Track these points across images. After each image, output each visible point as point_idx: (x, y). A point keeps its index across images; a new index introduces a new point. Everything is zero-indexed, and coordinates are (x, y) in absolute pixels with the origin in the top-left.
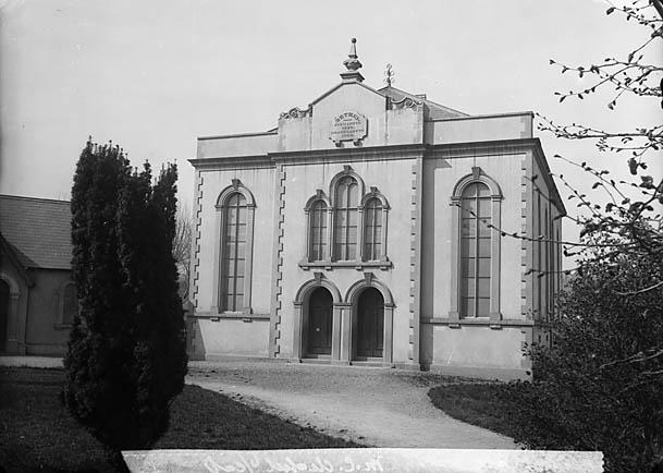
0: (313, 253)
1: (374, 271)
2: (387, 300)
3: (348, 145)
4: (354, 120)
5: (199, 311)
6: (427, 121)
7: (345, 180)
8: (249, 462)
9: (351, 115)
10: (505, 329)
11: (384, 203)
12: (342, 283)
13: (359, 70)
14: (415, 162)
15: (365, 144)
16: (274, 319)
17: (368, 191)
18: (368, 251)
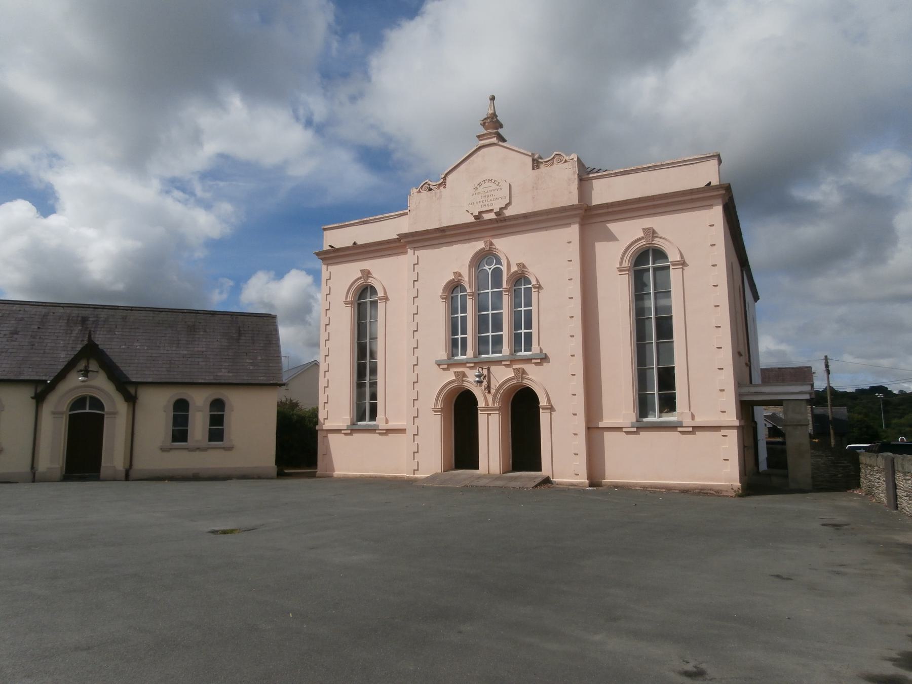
0: (456, 345)
1: (527, 367)
2: (543, 402)
3: (487, 217)
4: (494, 186)
5: (328, 425)
6: (585, 176)
7: (486, 255)
8: (45, 364)
9: (490, 181)
10: (699, 434)
11: (534, 282)
12: (261, 332)
13: (500, 131)
14: (573, 231)
15: (508, 213)
16: (411, 430)
17: (514, 268)
18: (522, 341)
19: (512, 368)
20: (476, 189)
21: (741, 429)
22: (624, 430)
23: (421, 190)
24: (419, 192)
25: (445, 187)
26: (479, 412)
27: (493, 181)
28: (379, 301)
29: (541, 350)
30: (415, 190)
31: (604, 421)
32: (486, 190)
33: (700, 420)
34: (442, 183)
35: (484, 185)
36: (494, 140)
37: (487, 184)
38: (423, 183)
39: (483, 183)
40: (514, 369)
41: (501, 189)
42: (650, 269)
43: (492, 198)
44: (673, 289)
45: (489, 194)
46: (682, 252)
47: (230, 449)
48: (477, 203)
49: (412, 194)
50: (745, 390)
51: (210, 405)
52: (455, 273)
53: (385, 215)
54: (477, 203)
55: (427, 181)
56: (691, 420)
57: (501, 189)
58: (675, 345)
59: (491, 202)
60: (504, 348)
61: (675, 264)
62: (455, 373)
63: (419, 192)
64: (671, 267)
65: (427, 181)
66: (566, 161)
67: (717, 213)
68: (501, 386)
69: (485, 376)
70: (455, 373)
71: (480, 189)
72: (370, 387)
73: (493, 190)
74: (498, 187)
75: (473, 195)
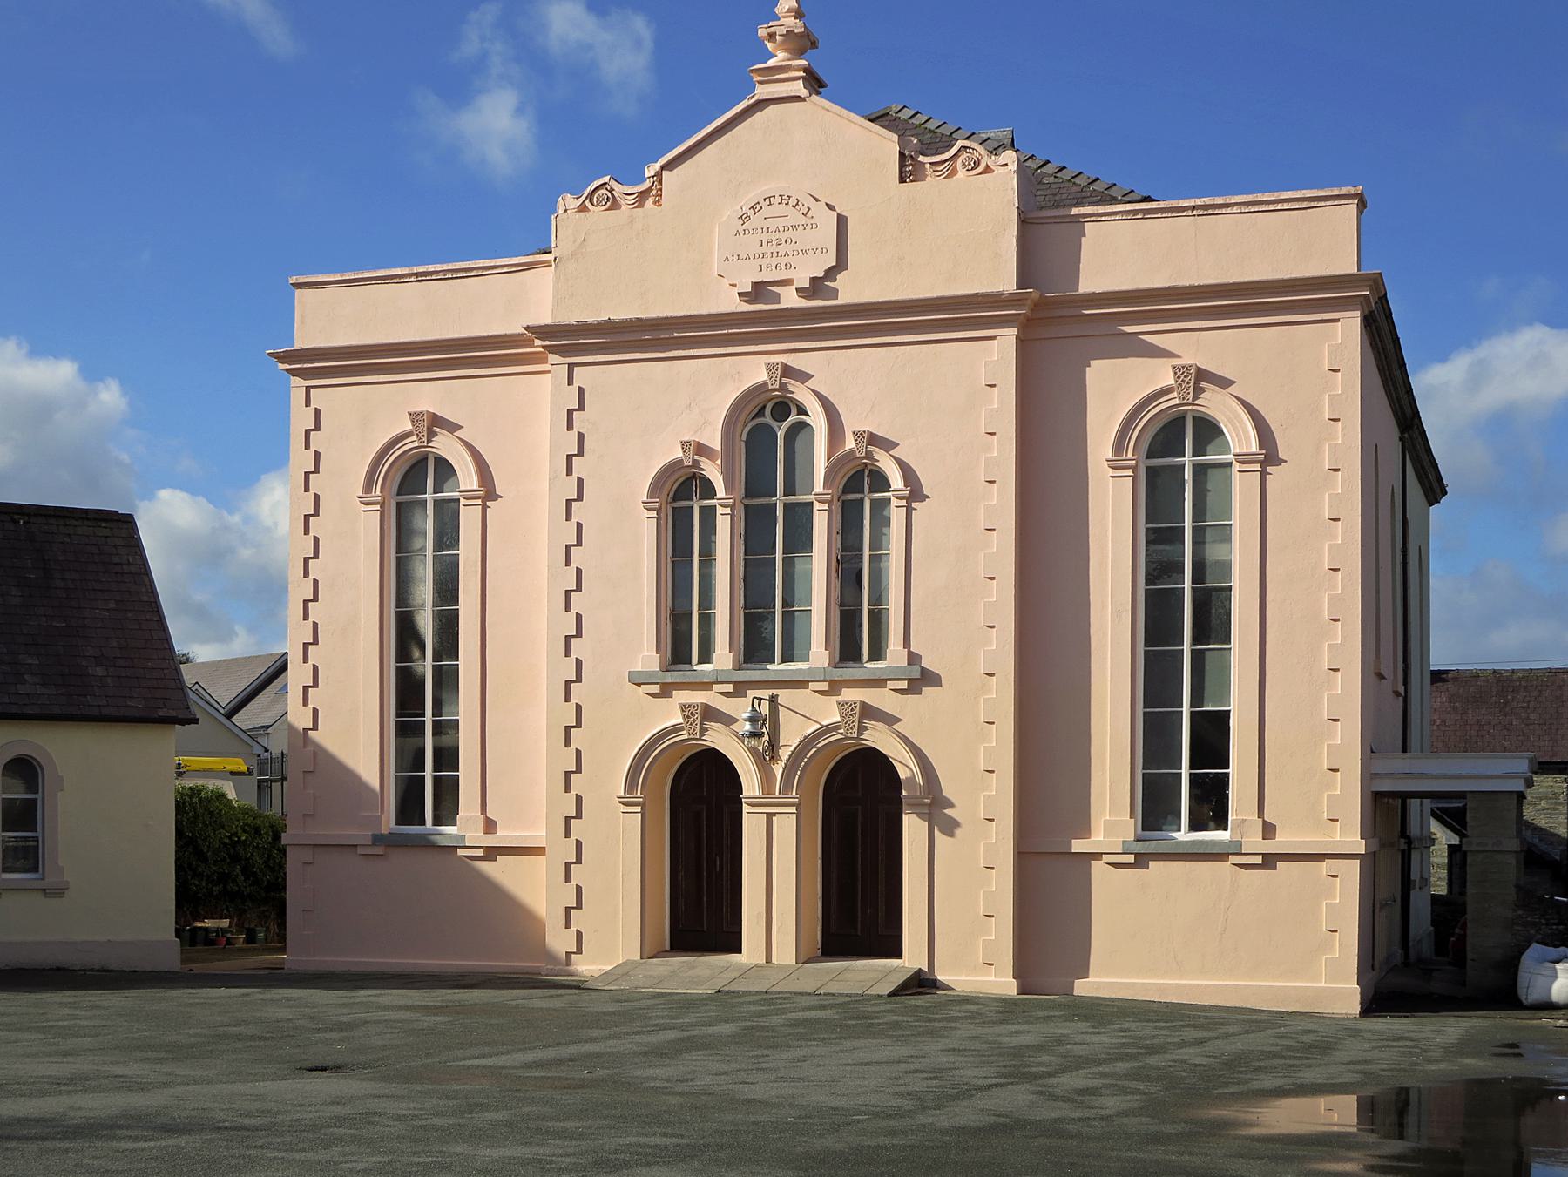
4: (795, 217)
19: (808, 691)
20: (744, 218)
21: (1370, 863)
22: (360, 851)
23: (587, 202)
24: (582, 208)
25: (657, 203)
26: (746, 808)
27: (793, 202)
28: (462, 502)
29: (913, 658)
30: (572, 202)
31: (1092, 839)
32: (773, 224)
33: (1284, 841)
34: (650, 189)
35: (767, 211)
36: (799, 88)
37: (777, 209)
38: (596, 184)
39: (765, 204)
40: (841, 705)
41: (814, 226)
42: (1184, 465)
43: (789, 247)
44: (1235, 521)
45: (784, 236)
46: (1238, 395)
47: (59, 892)
48: (748, 257)
49: (561, 212)
50: (1380, 766)
51: (4, 768)
52: (685, 445)
53: (481, 263)
54: (748, 257)
55: (606, 179)
56: (1261, 839)
57: (814, 226)
58: (1347, 737)
59: (786, 260)
60: (814, 648)
61: (1244, 459)
62: (683, 707)
63: (582, 208)
64: (1236, 467)
65: (606, 179)
66: (988, 170)
67: (1348, 329)
68: (808, 742)
69: (765, 720)
70: (683, 707)
71: (756, 221)
72: (433, 735)
73: (795, 227)
74: (804, 220)
75: (738, 233)
